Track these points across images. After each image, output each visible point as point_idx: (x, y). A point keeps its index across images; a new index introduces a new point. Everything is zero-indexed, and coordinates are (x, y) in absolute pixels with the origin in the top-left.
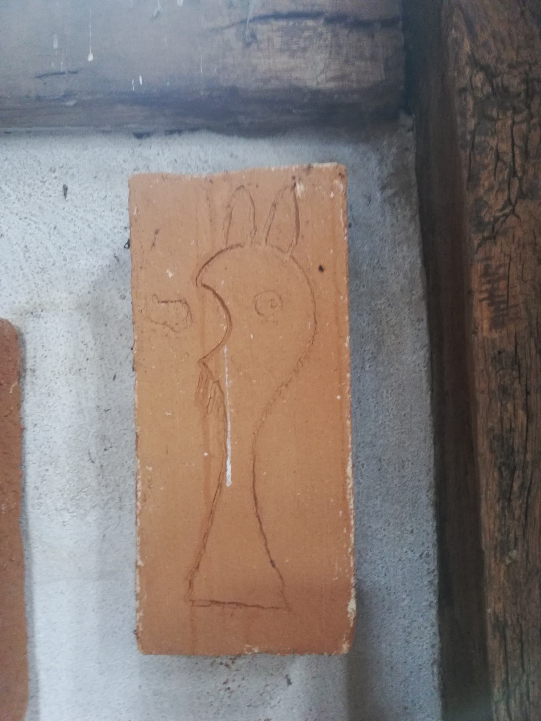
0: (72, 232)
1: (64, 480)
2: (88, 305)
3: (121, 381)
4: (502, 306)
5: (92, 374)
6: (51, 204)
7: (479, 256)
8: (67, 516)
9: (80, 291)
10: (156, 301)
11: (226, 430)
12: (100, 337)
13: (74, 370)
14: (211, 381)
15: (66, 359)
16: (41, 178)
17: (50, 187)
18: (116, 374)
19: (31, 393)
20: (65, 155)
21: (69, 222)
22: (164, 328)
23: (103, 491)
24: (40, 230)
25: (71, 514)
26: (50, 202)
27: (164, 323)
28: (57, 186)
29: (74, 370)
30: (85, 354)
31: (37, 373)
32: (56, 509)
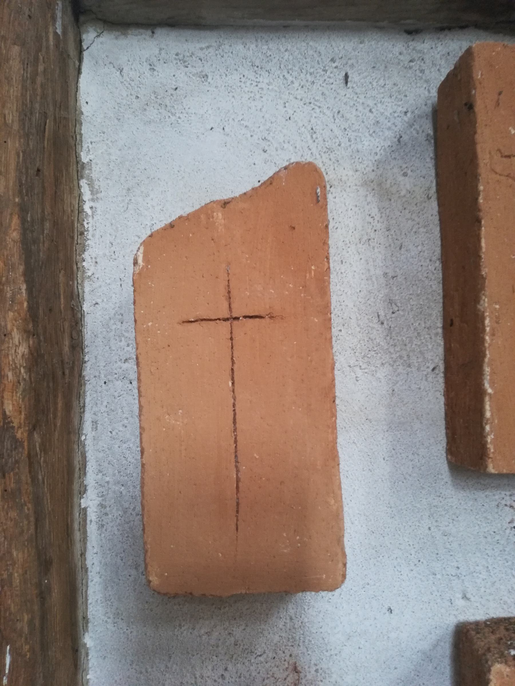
1: (356, 340)
2: (372, 182)
5: (380, 244)
6: (333, 91)
8: (359, 373)
9: (365, 169)
10: (499, 155)
12: (385, 210)
13: (363, 240)
15: (355, 230)
16: (322, 68)
17: (332, 75)
18: (402, 243)
20: (344, 47)
22: (507, 179)
23: (392, 350)
25: (363, 370)
26: (331, 89)
27: (508, 176)
28: (338, 75)
29: (363, 240)
30: (373, 226)
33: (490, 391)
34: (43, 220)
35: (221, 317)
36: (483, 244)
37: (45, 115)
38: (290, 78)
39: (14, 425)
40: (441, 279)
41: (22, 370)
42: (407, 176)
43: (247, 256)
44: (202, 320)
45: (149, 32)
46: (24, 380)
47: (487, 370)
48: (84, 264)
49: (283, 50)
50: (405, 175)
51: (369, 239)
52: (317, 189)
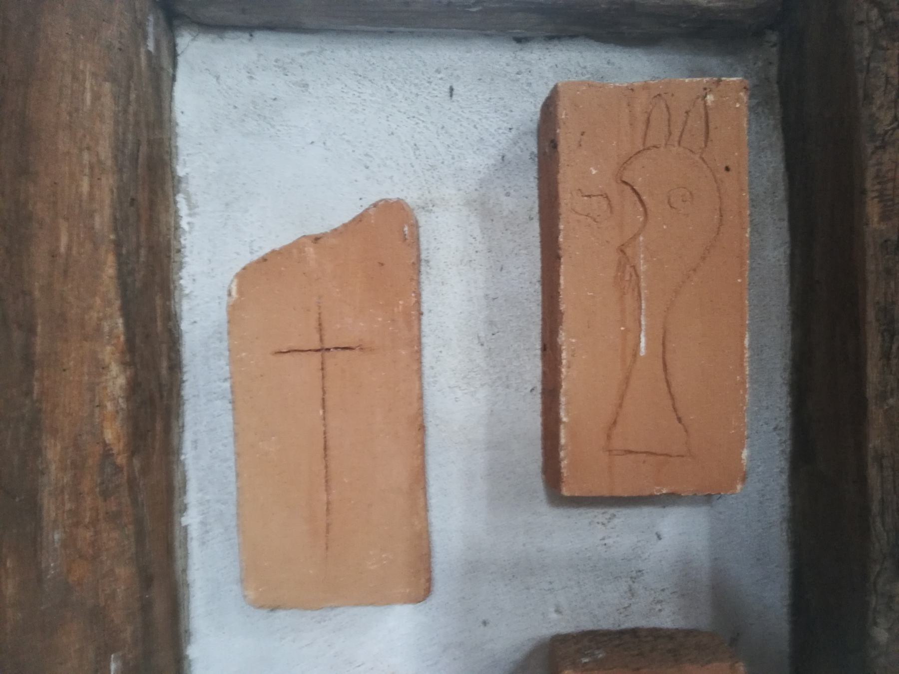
0: (459, 132)
3: (507, 272)
4: (889, 203)
7: (872, 162)
8: (459, 393)
11: (640, 308)
14: (628, 266)
15: (457, 251)
17: (436, 87)
18: (502, 265)
19: (426, 282)
21: (455, 122)
24: (428, 129)
31: (431, 263)
32: (449, 387)
33: (565, 419)
34: (139, 246)
35: (312, 348)
36: (562, 281)
37: (138, 143)
38: (394, 89)
39: (113, 452)
40: (540, 301)
41: (121, 400)
42: (509, 196)
43: (337, 290)
44: (296, 351)
45: (247, 35)
46: (122, 409)
47: (563, 399)
48: (182, 282)
49: (387, 57)
50: (508, 194)
51: (471, 261)
52: (403, 227)
